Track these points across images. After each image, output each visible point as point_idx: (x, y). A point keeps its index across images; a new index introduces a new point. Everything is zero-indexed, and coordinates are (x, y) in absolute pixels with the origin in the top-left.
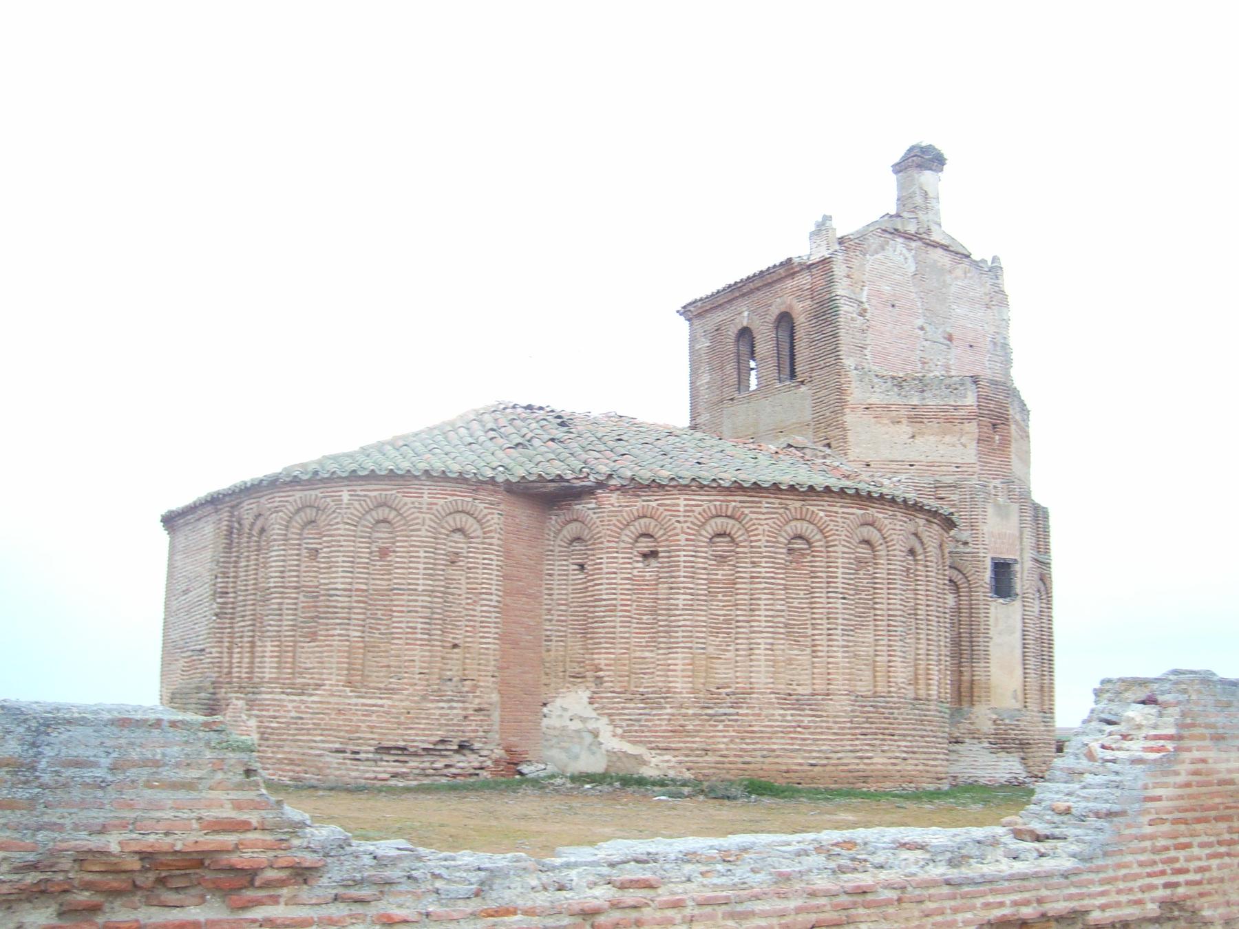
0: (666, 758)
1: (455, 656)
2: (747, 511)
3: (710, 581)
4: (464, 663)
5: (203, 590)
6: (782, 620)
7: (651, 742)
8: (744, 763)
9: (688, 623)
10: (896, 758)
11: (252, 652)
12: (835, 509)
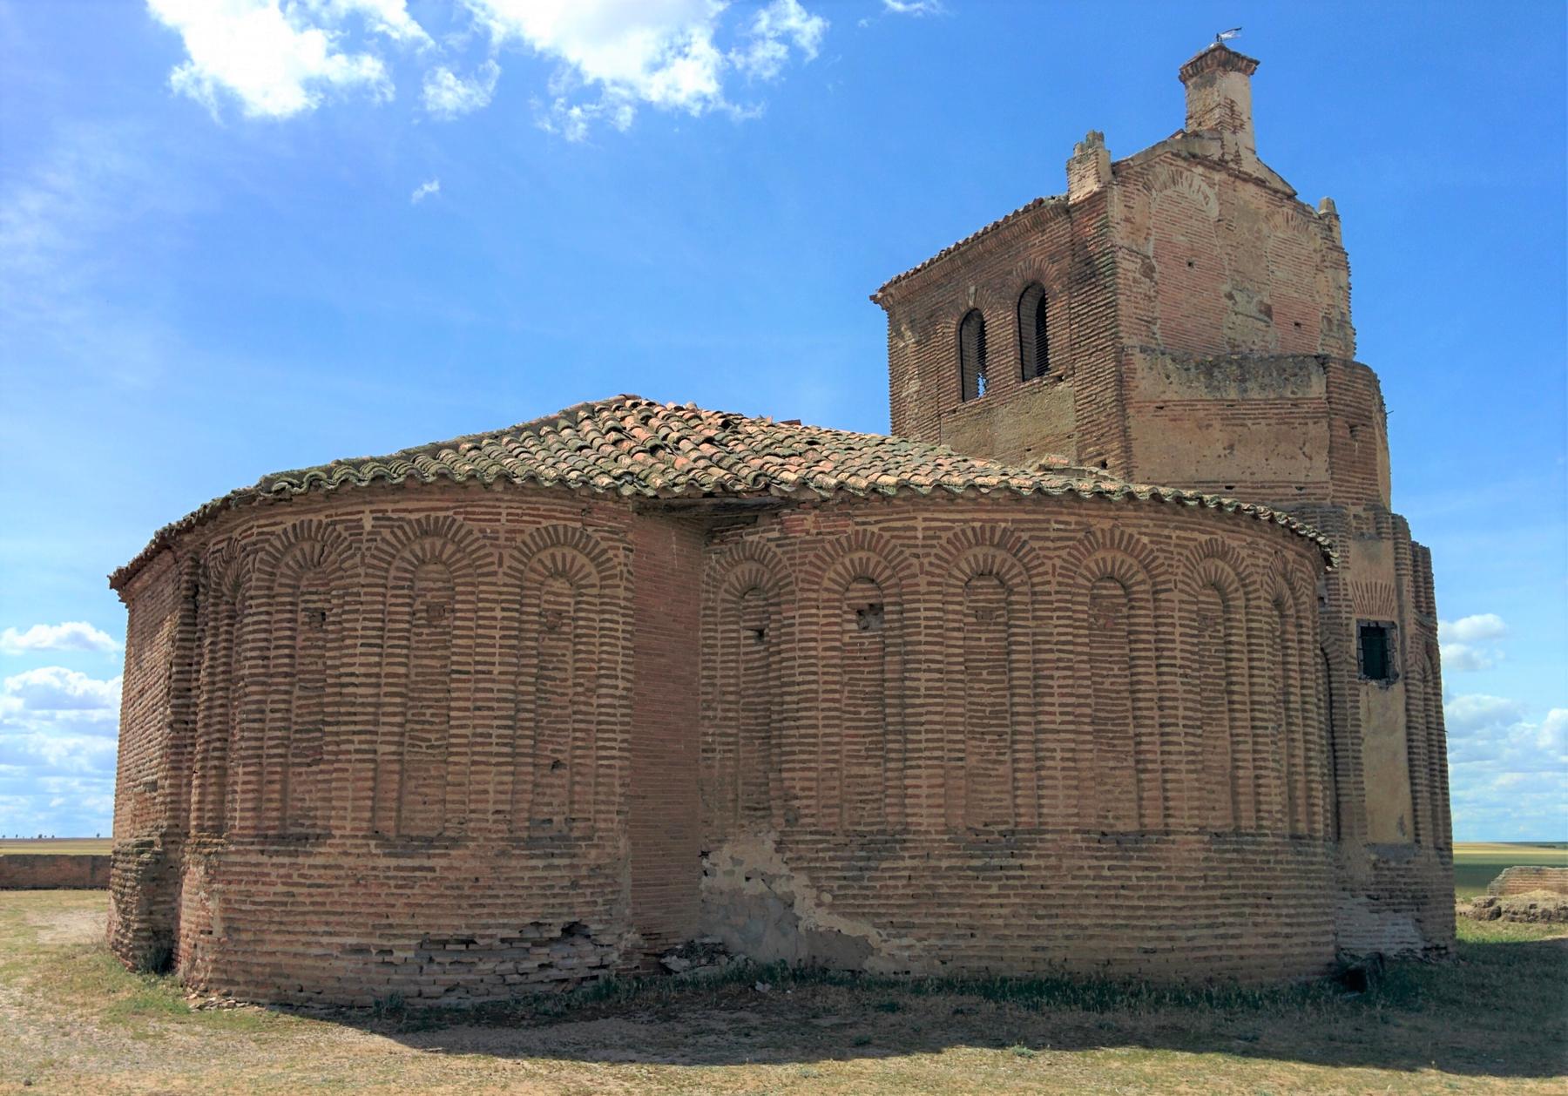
0: (905, 942)
1: (557, 782)
2: (1025, 536)
3: (969, 651)
4: (571, 792)
5: (158, 690)
6: (1088, 711)
7: (878, 915)
8: (1036, 949)
9: (937, 718)
10: (1276, 935)
11: (222, 785)
12: (1166, 532)
